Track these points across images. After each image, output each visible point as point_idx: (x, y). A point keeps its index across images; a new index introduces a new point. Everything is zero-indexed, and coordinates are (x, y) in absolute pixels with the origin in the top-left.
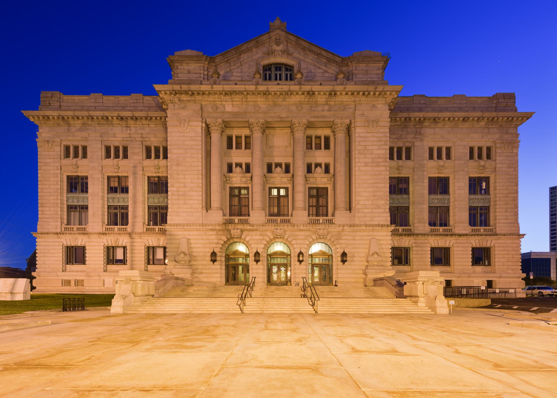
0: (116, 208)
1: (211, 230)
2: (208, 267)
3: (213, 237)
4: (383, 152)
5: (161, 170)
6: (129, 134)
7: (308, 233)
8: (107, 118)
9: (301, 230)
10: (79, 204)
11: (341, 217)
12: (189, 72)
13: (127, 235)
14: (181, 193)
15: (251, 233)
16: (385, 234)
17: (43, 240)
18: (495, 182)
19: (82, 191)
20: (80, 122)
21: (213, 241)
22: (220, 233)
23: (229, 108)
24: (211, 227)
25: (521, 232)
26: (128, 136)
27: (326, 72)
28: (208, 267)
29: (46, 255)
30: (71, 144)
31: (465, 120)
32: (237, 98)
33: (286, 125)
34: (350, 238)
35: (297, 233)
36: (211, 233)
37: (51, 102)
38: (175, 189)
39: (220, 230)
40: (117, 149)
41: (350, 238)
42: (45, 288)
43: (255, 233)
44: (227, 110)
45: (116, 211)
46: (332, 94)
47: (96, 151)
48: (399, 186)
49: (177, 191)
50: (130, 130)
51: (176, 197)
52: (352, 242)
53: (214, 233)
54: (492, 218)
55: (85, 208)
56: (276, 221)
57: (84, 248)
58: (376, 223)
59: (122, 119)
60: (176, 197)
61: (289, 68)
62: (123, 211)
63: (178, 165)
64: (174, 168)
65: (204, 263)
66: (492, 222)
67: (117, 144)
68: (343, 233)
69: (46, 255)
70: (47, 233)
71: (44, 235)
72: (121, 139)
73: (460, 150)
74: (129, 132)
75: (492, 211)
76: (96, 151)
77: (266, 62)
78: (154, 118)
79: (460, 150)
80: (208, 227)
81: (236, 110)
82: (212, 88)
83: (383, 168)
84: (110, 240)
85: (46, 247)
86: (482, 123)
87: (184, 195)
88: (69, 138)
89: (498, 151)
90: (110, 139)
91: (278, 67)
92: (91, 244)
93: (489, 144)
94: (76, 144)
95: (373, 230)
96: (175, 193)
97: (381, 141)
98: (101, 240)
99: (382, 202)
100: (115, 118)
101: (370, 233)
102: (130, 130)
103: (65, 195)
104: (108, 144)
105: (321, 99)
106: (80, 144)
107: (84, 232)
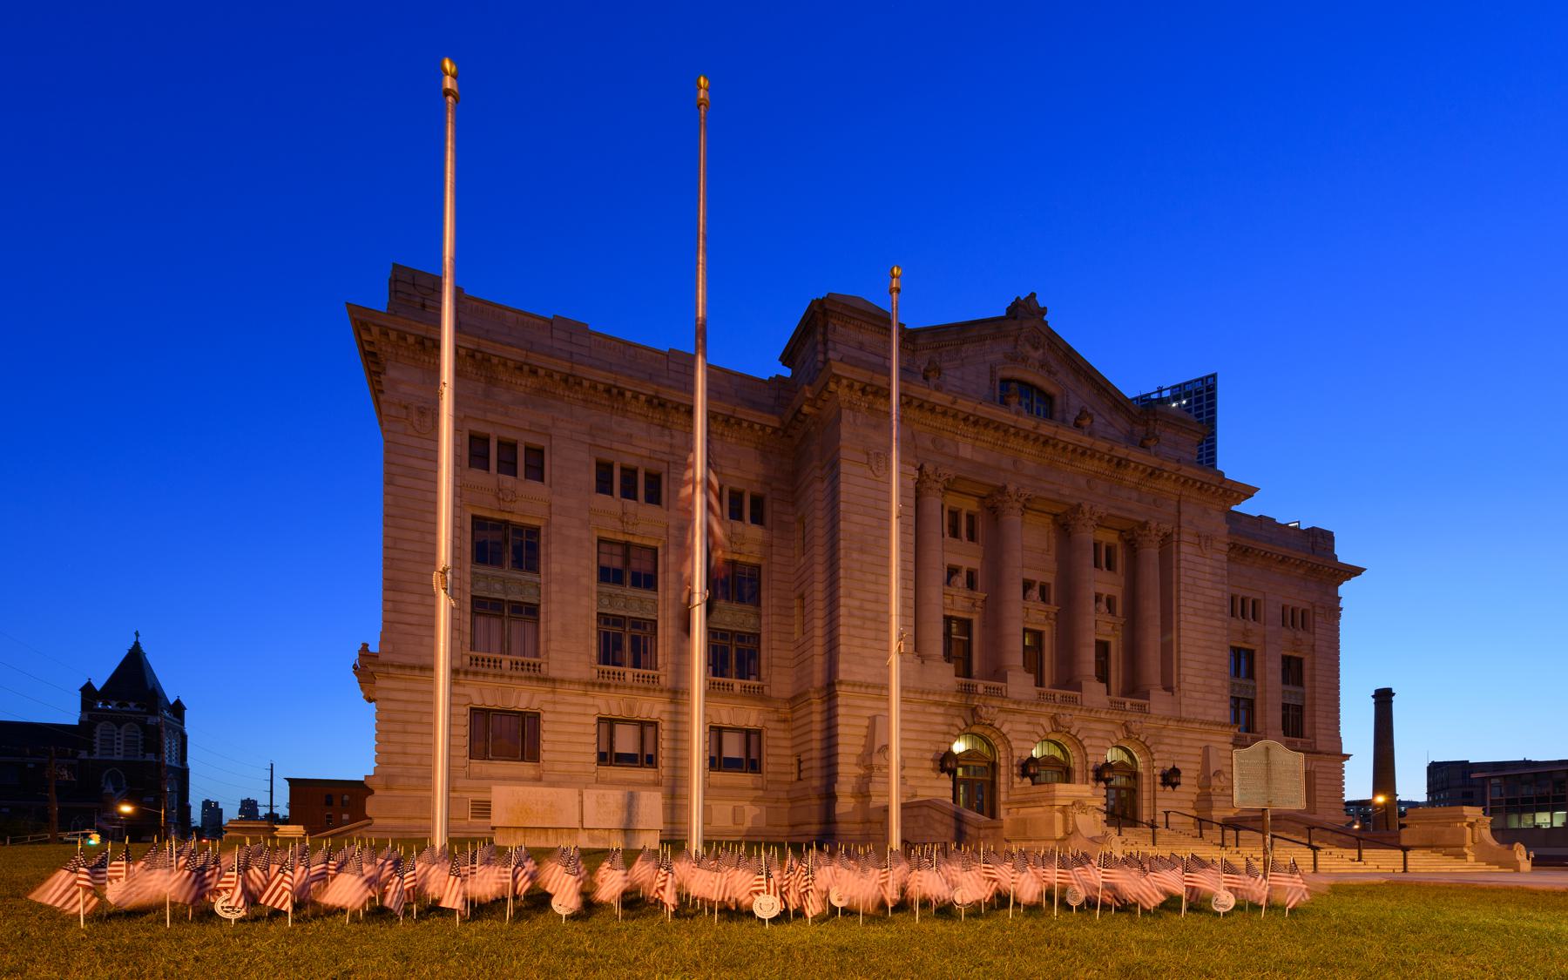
0: (618, 621)
1: (936, 704)
2: (928, 783)
3: (940, 719)
4: (1219, 594)
5: (745, 549)
6: (671, 446)
7: (1109, 727)
8: (621, 393)
9: (1100, 720)
10: (511, 597)
11: (1159, 702)
12: (861, 347)
13: (666, 695)
14: (868, 614)
15: (1011, 717)
16: (1224, 739)
17: (402, 685)
18: (1313, 669)
19: (518, 564)
20: (531, 381)
21: (938, 728)
22: (953, 711)
23: (966, 451)
24: (937, 698)
25: (1345, 751)
26: (667, 449)
27: (1111, 425)
28: (928, 783)
29: (410, 728)
30: (494, 434)
31: (1284, 560)
32: (989, 435)
33: (1047, 509)
34: (1175, 742)
35: (1092, 726)
36: (933, 709)
37: (428, 303)
38: (857, 603)
39: (952, 705)
40: (629, 475)
41: (1175, 742)
42: (407, 822)
43: (1018, 717)
44: (962, 453)
45: (617, 630)
46: (1154, 473)
47: (572, 464)
48: (1243, 661)
49: (861, 608)
50: (672, 436)
51: (858, 622)
52: (1178, 750)
53: (941, 710)
54: (1307, 726)
55: (530, 612)
56: (730, 686)
57: (535, 717)
58: (1211, 718)
59: (662, 405)
60: (858, 622)
61: (1048, 399)
62: (637, 632)
63: (862, 551)
64: (855, 555)
65: (920, 773)
66: (1307, 732)
67: (631, 462)
68: (1165, 733)
69: (410, 728)
70: (413, 667)
71: (408, 672)
72: (644, 452)
73: (1272, 610)
74: (667, 439)
75: (1307, 713)
76: (572, 464)
77: (1008, 374)
78: (745, 425)
79: (1272, 610)
80: (931, 697)
81: (980, 458)
82: (954, 403)
83: (1218, 624)
84: (611, 703)
85: (411, 707)
86: (1301, 571)
87: (875, 620)
88: (490, 417)
89: (1318, 619)
90: (616, 446)
91: (1027, 388)
92: (559, 708)
93: (1305, 606)
94: (510, 435)
95: (1207, 732)
96: (856, 612)
97: (1215, 574)
98: (590, 701)
99: (1217, 683)
100: (643, 398)
101: (1204, 736)
102: (672, 436)
103: (468, 567)
104: (607, 456)
105: (1131, 477)
106: (524, 439)
107: (535, 674)
